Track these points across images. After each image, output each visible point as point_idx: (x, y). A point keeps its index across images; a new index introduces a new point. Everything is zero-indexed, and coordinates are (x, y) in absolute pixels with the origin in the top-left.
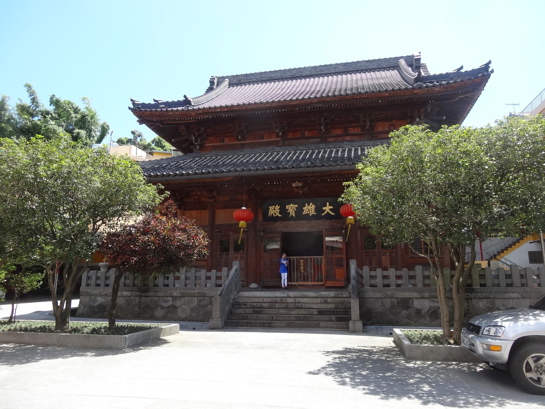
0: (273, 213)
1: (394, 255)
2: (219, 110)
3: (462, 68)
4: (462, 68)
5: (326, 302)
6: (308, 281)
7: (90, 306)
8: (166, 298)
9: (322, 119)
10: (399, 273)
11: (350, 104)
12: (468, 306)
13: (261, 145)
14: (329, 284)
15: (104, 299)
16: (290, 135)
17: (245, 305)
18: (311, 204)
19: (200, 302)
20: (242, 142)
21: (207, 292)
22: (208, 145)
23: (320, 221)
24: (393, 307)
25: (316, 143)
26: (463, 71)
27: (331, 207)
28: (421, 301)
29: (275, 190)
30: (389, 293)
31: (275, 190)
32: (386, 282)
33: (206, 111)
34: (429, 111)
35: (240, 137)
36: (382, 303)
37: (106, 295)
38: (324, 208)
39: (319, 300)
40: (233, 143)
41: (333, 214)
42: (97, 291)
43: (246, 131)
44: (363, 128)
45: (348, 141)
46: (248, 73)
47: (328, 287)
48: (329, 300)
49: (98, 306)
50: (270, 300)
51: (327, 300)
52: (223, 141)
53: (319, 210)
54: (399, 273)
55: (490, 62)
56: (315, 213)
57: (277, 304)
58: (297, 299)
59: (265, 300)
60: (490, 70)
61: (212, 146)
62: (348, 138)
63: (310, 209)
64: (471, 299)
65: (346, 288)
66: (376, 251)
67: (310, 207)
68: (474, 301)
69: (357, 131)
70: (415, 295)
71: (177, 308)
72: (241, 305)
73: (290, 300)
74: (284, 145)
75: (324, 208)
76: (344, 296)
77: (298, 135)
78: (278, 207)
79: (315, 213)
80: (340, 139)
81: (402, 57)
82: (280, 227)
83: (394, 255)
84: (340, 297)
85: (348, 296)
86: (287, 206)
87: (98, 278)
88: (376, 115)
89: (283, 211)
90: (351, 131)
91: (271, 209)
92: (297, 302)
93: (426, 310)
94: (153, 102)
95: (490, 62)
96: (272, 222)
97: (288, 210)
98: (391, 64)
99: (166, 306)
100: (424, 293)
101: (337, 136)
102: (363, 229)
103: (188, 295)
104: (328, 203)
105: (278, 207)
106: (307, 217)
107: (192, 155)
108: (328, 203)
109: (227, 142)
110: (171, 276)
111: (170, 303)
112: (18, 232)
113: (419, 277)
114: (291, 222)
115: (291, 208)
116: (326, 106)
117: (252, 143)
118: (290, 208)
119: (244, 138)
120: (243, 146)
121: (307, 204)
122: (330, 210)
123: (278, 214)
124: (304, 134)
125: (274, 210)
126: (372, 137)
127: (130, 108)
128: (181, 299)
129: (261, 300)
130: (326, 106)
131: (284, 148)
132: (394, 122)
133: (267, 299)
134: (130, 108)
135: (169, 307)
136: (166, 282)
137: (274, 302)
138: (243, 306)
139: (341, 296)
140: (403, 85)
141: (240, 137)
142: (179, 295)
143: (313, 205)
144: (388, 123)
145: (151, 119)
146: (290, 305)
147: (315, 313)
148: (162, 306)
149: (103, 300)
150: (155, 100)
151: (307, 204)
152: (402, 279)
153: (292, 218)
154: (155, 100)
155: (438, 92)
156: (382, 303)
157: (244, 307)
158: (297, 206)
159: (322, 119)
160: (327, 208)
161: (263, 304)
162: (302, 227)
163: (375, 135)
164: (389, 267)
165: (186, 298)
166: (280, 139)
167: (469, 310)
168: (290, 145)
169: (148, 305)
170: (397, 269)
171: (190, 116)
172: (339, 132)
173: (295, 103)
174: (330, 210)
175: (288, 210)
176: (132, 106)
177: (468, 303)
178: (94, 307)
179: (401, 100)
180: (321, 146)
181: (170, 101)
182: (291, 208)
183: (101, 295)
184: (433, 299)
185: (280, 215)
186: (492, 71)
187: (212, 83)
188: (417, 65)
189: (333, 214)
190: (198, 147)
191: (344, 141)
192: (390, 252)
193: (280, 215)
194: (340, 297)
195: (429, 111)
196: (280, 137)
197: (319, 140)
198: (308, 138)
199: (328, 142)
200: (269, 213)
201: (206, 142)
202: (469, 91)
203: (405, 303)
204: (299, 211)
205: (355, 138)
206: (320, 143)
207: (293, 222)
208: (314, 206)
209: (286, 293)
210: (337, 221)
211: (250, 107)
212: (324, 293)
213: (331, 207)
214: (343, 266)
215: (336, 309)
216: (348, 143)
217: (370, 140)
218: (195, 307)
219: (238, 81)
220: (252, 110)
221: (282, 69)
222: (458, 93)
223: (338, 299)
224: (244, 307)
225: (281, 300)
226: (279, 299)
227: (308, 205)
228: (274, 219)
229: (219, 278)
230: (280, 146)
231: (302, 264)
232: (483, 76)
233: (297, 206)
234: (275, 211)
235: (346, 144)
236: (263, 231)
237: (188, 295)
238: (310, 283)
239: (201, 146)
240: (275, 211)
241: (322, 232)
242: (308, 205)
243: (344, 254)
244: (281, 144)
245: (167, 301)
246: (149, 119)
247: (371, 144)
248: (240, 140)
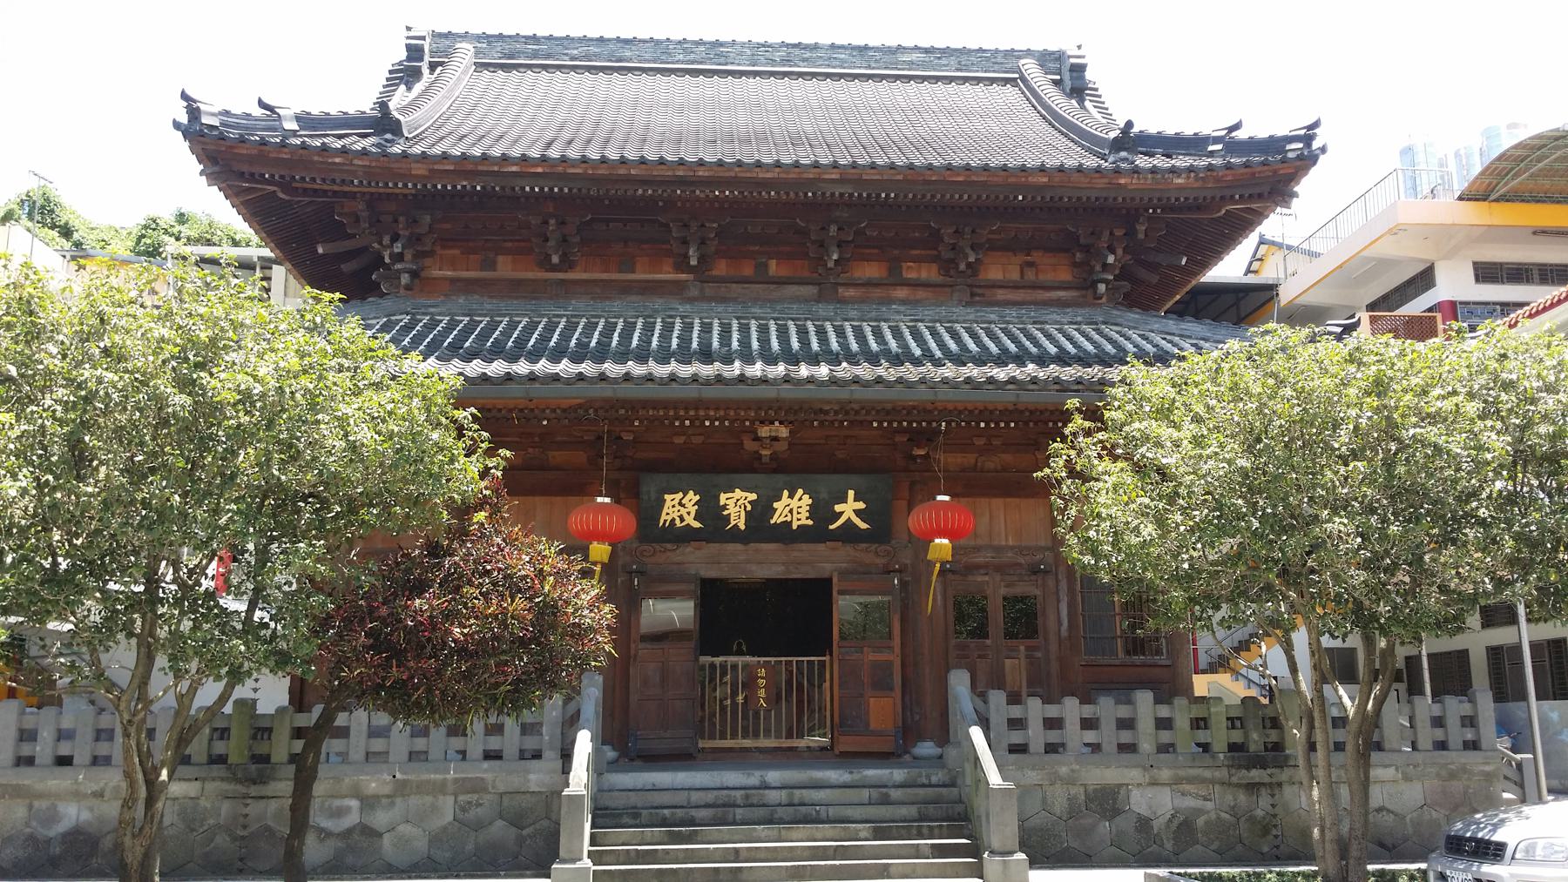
0: (676, 515)
1: (1039, 654)
2: (514, 169)
3: (1237, 127)
4: (1237, 127)
5: (885, 801)
6: (756, 735)
7: (32, 838)
8: (337, 803)
9: (833, 229)
10: (1052, 711)
11: (933, 196)
12: (1273, 806)
13: (626, 289)
14: (846, 744)
15: (91, 809)
16: (721, 268)
17: (636, 816)
18: (800, 491)
19: (463, 810)
20: (561, 276)
21: (489, 776)
22: (437, 273)
23: (821, 547)
24: (1073, 812)
25: (806, 301)
26: (1241, 135)
27: (861, 505)
28: (1150, 792)
29: (679, 440)
30: (1064, 770)
31: (679, 440)
32: (1054, 736)
33: (470, 167)
34: (1141, 236)
35: (555, 259)
36: (1044, 800)
37: (99, 795)
38: (838, 508)
39: (865, 794)
40: (530, 275)
41: (863, 525)
42: (59, 781)
43: (577, 239)
44: (948, 266)
45: (903, 302)
46: (725, 37)
47: (844, 755)
48: (895, 794)
49: (65, 835)
50: (710, 797)
51: (887, 795)
52: (492, 266)
53: (822, 512)
54: (1052, 711)
55: (1316, 125)
56: (810, 522)
57: (739, 811)
58: (797, 792)
59: (696, 797)
60: (1316, 145)
61: (453, 281)
62: (901, 293)
63: (793, 508)
64: (1280, 785)
65: (899, 756)
66: (988, 642)
67: (794, 503)
68: (1288, 791)
69: (928, 273)
70: (1134, 775)
71: (380, 835)
72: (620, 815)
73: (773, 796)
74: (703, 298)
75: (838, 508)
76: (934, 779)
77: (748, 270)
78: (692, 497)
79: (810, 522)
80: (877, 293)
81: (1029, 53)
82: (702, 561)
83: (1039, 654)
84: (923, 786)
85: (947, 779)
86: (723, 498)
87: (62, 735)
88: (992, 232)
89: (710, 512)
90: (911, 272)
91: (668, 504)
92: (796, 801)
93: (1162, 820)
94: (258, 112)
95: (1316, 125)
96: (669, 546)
97: (725, 507)
98: (999, 67)
99: (337, 830)
100: (1159, 768)
101: (870, 284)
102: (950, 576)
103: (422, 788)
104: (851, 493)
105: (692, 497)
106: (785, 534)
107: (387, 303)
108: (851, 493)
109: (505, 268)
110: (477, 726)
111: (352, 819)
112: (191, 572)
113: (1146, 724)
114: (731, 547)
115: (736, 504)
116: (860, 195)
117: (594, 281)
118: (731, 503)
119: (567, 264)
120: (567, 290)
121: (786, 493)
122: (857, 512)
123: (691, 521)
124: (766, 266)
125: (680, 508)
126: (973, 295)
127: (177, 125)
128: (392, 804)
129: (680, 798)
130: (860, 195)
131: (705, 306)
132: (1036, 256)
133: (701, 794)
134: (177, 125)
135: (349, 832)
136: (494, 743)
137: (724, 805)
138: (626, 820)
139: (925, 781)
140: (1071, 156)
141: (555, 259)
142: (387, 790)
143: (806, 497)
144: (1021, 258)
145: (257, 170)
146: (781, 812)
147: (862, 834)
148: (321, 830)
149: (86, 816)
150: (262, 104)
151: (786, 493)
152: (1171, 728)
153: (735, 535)
154: (262, 104)
155: (1180, 188)
156: (1044, 800)
157: (631, 822)
158: (753, 496)
159: (833, 229)
160: (849, 509)
161: (693, 812)
162: (766, 563)
163: (979, 291)
164: (1024, 694)
165: (415, 801)
166: (691, 277)
167: (1275, 816)
168: (723, 300)
169: (268, 829)
170: (1047, 700)
171: (406, 177)
172: (871, 271)
173: (769, 175)
174: (857, 512)
175: (725, 507)
176: (184, 119)
177: (1273, 796)
178: (49, 841)
179: (1079, 199)
180: (822, 309)
181: (315, 111)
182: (736, 504)
183: (77, 795)
184: (1181, 787)
185: (697, 525)
186: (1323, 150)
187: (415, 52)
188: (1078, 84)
189: (863, 525)
190: (405, 279)
191: (889, 301)
192: (1028, 648)
193: (697, 525)
194: (923, 786)
195: (1141, 236)
196: (690, 270)
197: (811, 290)
198: (781, 282)
199: (843, 301)
200: (664, 517)
201: (428, 262)
202: (1260, 196)
203: (1107, 801)
204: (760, 513)
205: (921, 294)
206: (818, 301)
207: (739, 546)
208: (807, 500)
209: (758, 773)
210: (874, 546)
211: (622, 171)
212: (872, 773)
213: (861, 505)
214: (892, 689)
215: (921, 820)
216: (902, 308)
217: (968, 304)
218: (445, 829)
219: (509, 54)
220: (628, 180)
221: (659, 35)
222: (1232, 197)
223: (921, 791)
224: (631, 822)
225: (747, 797)
226: (739, 794)
227: (791, 496)
228: (684, 536)
229: (1126, 724)
230: (691, 300)
231: (762, 682)
232: (1300, 158)
233: (753, 496)
234: (683, 511)
235: (898, 312)
236: (640, 573)
237: (422, 788)
238: (764, 743)
239: (414, 274)
240: (683, 511)
241: (829, 580)
242: (791, 496)
243: (897, 650)
244: (694, 292)
245: (340, 813)
246: (245, 168)
247: (971, 317)
248: (554, 269)
